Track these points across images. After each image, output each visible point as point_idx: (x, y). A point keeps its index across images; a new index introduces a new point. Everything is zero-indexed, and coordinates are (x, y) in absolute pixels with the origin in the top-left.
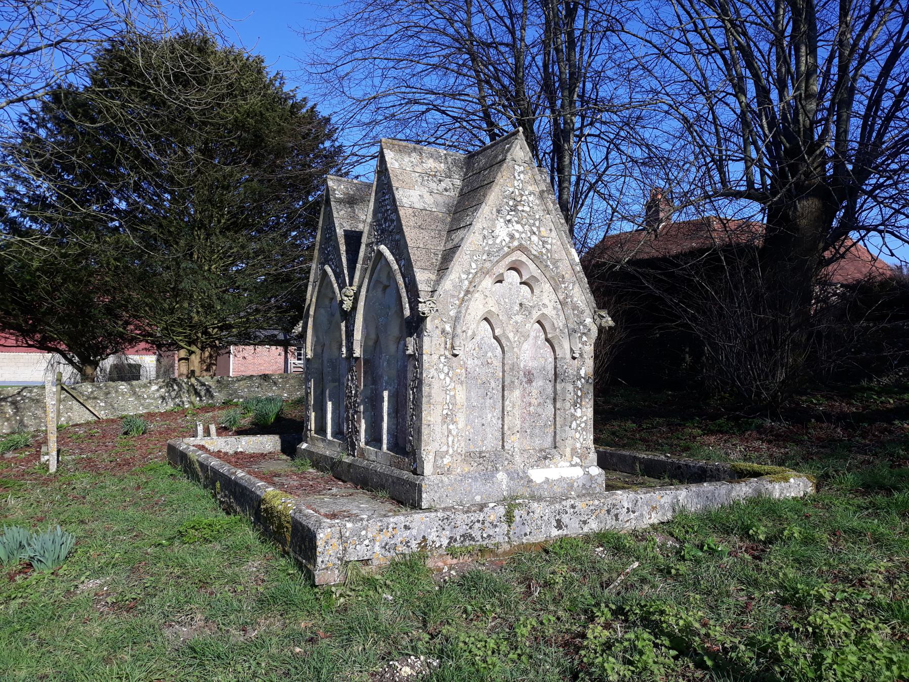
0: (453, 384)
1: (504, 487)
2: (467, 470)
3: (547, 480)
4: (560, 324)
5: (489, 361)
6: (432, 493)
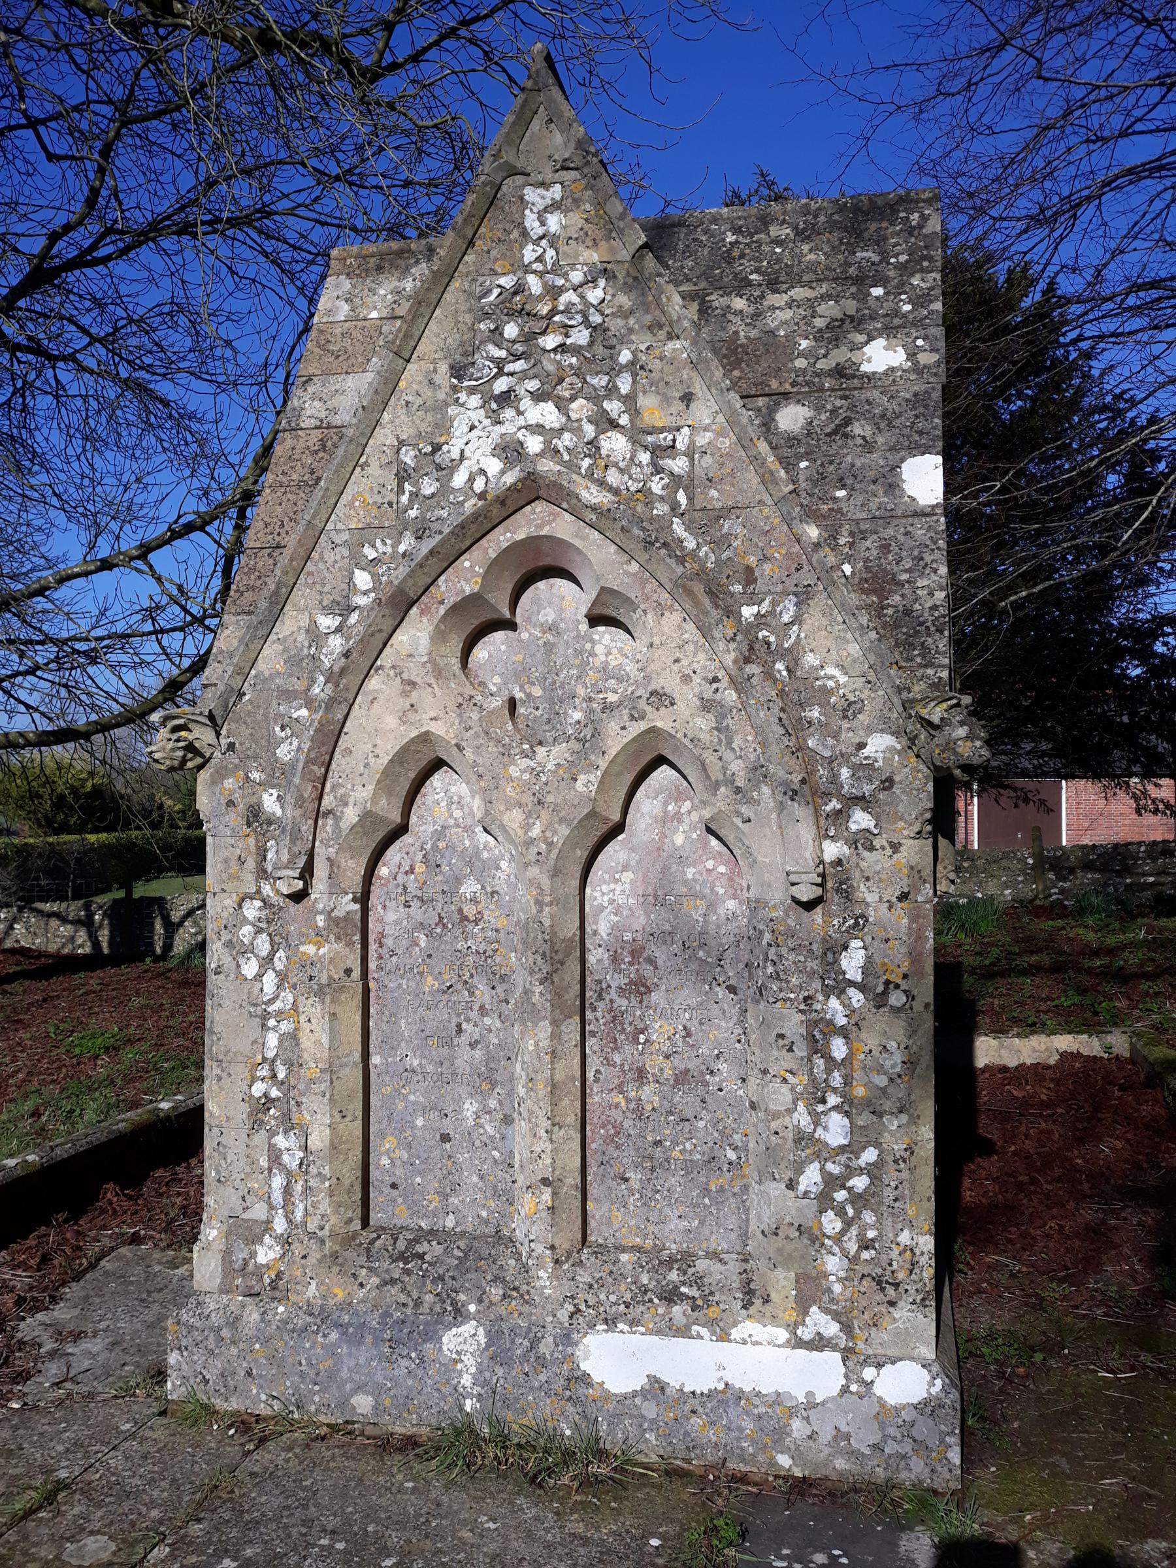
0: (288, 996)
1: (466, 1380)
2: (340, 1294)
3: (656, 1388)
4: (736, 766)
5: (470, 910)
6: (199, 1357)
